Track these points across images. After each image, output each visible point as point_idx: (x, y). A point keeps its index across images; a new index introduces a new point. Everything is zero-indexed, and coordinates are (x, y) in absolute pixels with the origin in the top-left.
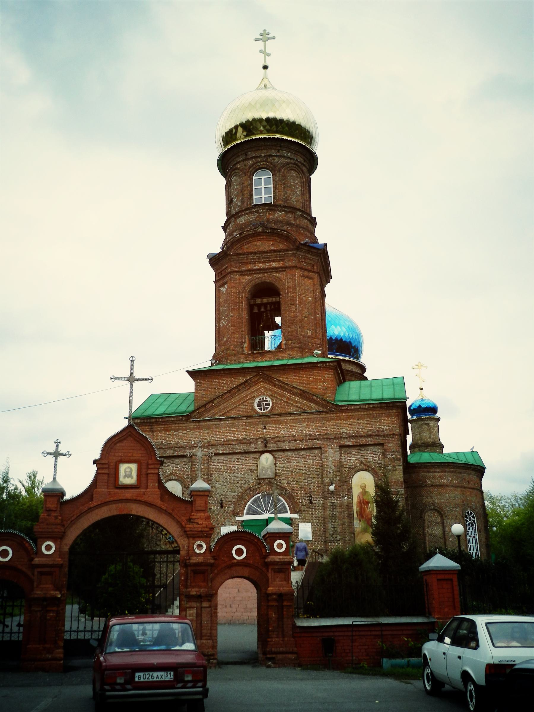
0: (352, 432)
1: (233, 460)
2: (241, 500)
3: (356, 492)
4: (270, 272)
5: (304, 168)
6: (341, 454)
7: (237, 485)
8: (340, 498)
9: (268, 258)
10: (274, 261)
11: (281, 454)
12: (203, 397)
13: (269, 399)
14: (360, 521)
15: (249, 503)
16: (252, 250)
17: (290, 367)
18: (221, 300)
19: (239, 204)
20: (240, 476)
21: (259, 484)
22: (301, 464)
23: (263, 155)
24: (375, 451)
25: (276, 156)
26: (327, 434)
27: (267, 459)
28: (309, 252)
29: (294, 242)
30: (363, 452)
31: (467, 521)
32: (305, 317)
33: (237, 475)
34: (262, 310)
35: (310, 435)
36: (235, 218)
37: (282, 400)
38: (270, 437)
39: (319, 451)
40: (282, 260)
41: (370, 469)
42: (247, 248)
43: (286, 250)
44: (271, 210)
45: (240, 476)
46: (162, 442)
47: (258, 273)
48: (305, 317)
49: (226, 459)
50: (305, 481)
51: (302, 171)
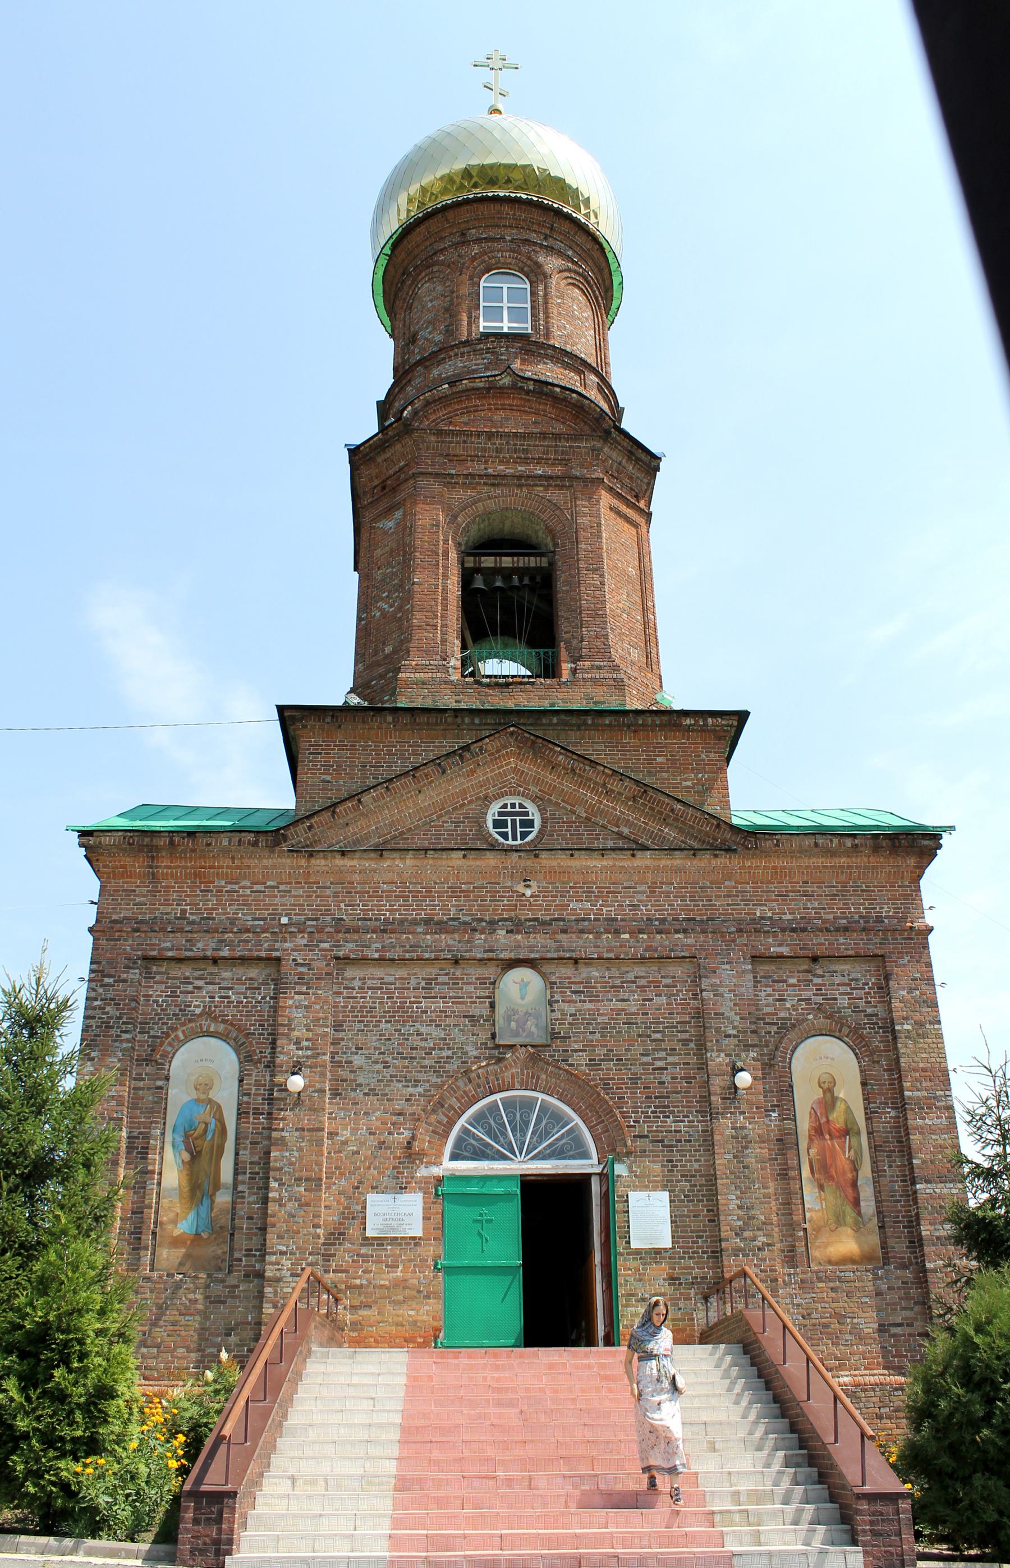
0: (789, 917)
1: (413, 982)
7: (426, 1062)
9: (526, 451)
10: (539, 461)
11: (567, 971)
12: (324, 789)
13: (531, 808)
14: (821, 1187)
15: (462, 1122)
20: (437, 1033)
23: (508, 238)
24: (856, 980)
25: (541, 246)
26: (712, 919)
27: (524, 985)
29: (597, 420)
30: (819, 981)
33: (424, 1030)
35: (663, 921)
37: (573, 812)
38: (536, 919)
40: (565, 462)
41: (845, 1030)
44: (528, 352)
45: (437, 1033)
47: (493, 485)
49: (389, 979)
50: (645, 1059)
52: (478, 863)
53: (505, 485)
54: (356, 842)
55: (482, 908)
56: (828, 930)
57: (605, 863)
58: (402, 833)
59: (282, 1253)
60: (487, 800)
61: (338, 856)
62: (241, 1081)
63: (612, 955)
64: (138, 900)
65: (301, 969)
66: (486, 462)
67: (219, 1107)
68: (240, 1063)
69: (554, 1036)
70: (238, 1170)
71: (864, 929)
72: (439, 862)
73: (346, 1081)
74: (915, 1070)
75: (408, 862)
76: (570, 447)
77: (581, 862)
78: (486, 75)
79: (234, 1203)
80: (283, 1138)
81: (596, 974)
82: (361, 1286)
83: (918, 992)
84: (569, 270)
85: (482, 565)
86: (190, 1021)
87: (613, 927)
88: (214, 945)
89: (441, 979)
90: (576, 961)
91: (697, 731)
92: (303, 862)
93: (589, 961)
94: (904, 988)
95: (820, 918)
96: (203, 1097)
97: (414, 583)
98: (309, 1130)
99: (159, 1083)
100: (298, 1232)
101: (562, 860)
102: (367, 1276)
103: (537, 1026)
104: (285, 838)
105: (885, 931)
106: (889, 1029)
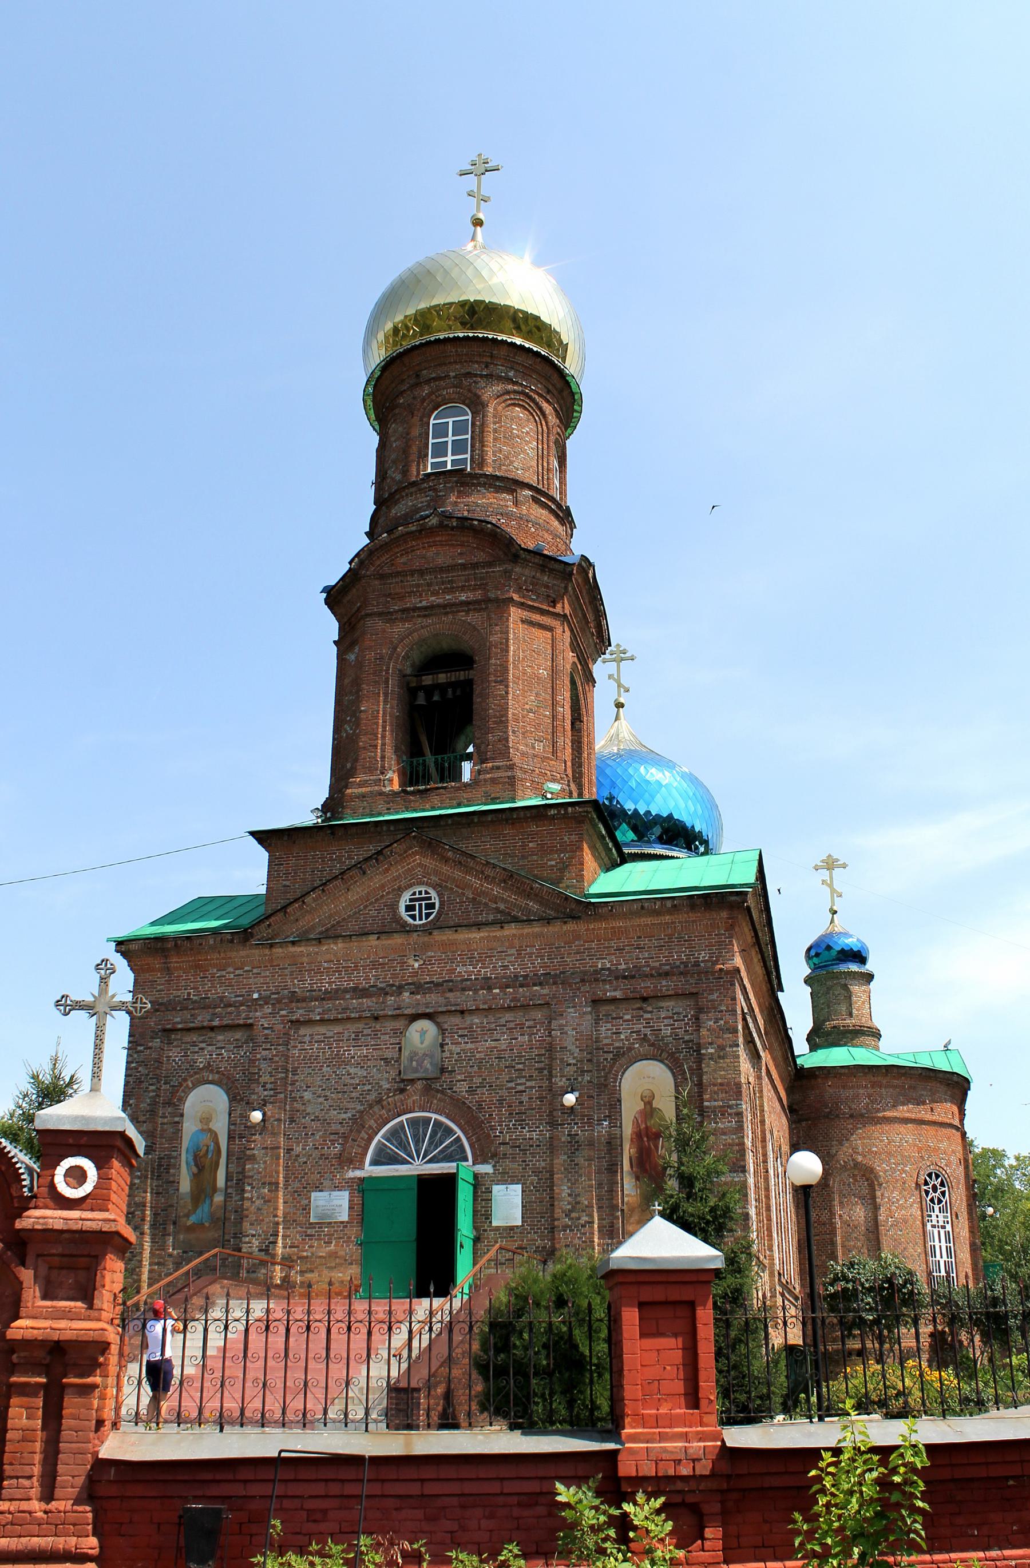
0: (623, 966)
1: (346, 1034)
2: (358, 1130)
3: (630, 1109)
4: (452, 612)
5: (545, 405)
6: (597, 1021)
7: (354, 1095)
8: (590, 1124)
10: (463, 589)
11: (456, 1020)
14: (637, 1178)
15: (378, 1137)
16: (416, 565)
17: (484, 819)
18: (346, 681)
19: (398, 478)
21: (402, 1091)
22: (503, 1044)
23: (452, 374)
24: (678, 1013)
25: (481, 376)
26: (563, 973)
27: (423, 1033)
28: (543, 568)
30: (649, 1016)
31: (927, 1193)
32: (530, 711)
33: (352, 1071)
34: (436, 698)
35: (525, 977)
36: (388, 507)
37: (464, 894)
38: (432, 982)
39: (545, 1011)
40: (483, 587)
41: (665, 1055)
42: (405, 564)
43: (490, 564)
44: (463, 484)
46: (189, 994)
47: (425, 616)
48: (530, 711)
50: (510, 1085)
51: (540, 409)
52: (389, 942)
53: (435, 615)
54: (306, 932)
55: (394, 976)
56: (652, 975)
57: (482, 935)
58: (338, 922)
59: (253, 1236)
60: (400, 890)
61: (290, 945)
62: (230, 1115)
63: (486, 1007)
64: (159, 988)
65: (266, 1032)
66: (421, 595)
67: (216, 1135)
68: (230, 1101)
69: (443, 1070)
70: (228, 1178)
71: (681, 973)
72: (362, 944)
73: (298, 1111)
74: (714, 1085)
75: (340, 945)
76: (487, 572)
77: (463, 935)
78: (471, 181)
79: (225, 1201)
80: (254, 1155)
81: (477, 1021)
82: (307, 1257)
83: (722, 1022)
84: (508, 392)
85: (423, 684)
86: (196, 1073)
87: (487, 984)
88: (209, 1018)
89: (366, 1032)
90: (462, 1012)
91: (560, 818)
92: (267, 951)
93: (471, 1012)
94: (711, 1020)
95: (648, 966)
96: (205, 1127)
97: (361, 711)
98: (272, 1148)
99: (177, 1119)
100: (263, 1220)
101: (448, 935)
102: (311, 1250)
103: (431, 1064)
104: (252, 935)
105: (699, 973)
106: (696, 1049)
